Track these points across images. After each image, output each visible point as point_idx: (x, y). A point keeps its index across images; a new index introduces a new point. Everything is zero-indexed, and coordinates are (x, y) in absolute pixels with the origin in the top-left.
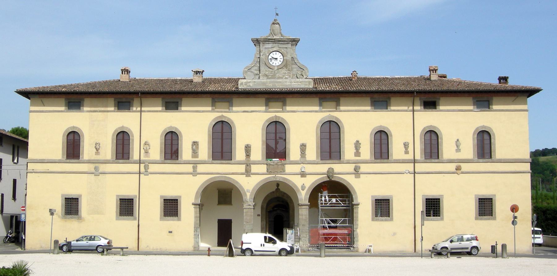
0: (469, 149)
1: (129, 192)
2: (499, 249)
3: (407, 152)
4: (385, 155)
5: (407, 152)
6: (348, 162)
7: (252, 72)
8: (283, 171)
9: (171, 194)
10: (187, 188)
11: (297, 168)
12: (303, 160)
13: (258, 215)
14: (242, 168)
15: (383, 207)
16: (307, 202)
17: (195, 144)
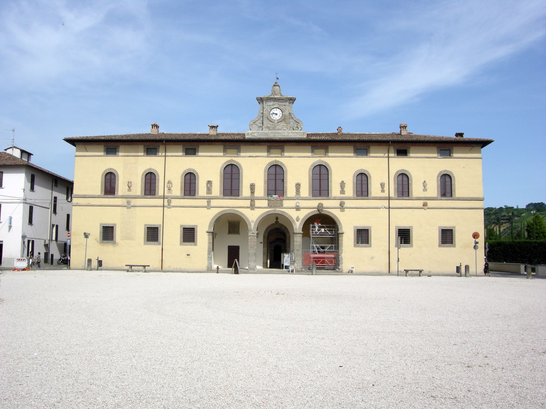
0: (433, 190)
1: (154, 222)
2: (463, 270)
3: (383, 191)
4: (448, 194)
5: (383, 191)
6: (335, 199)
7: (256, 125)
8: (281, 206)
9: (189, 223)
10: (203, 219)
11: (292, 203)
12: (298, 197)
13: (261, 243)
14: (248, 203)
15: (363, 236)
16: (301, 231)
17: (209, 182)
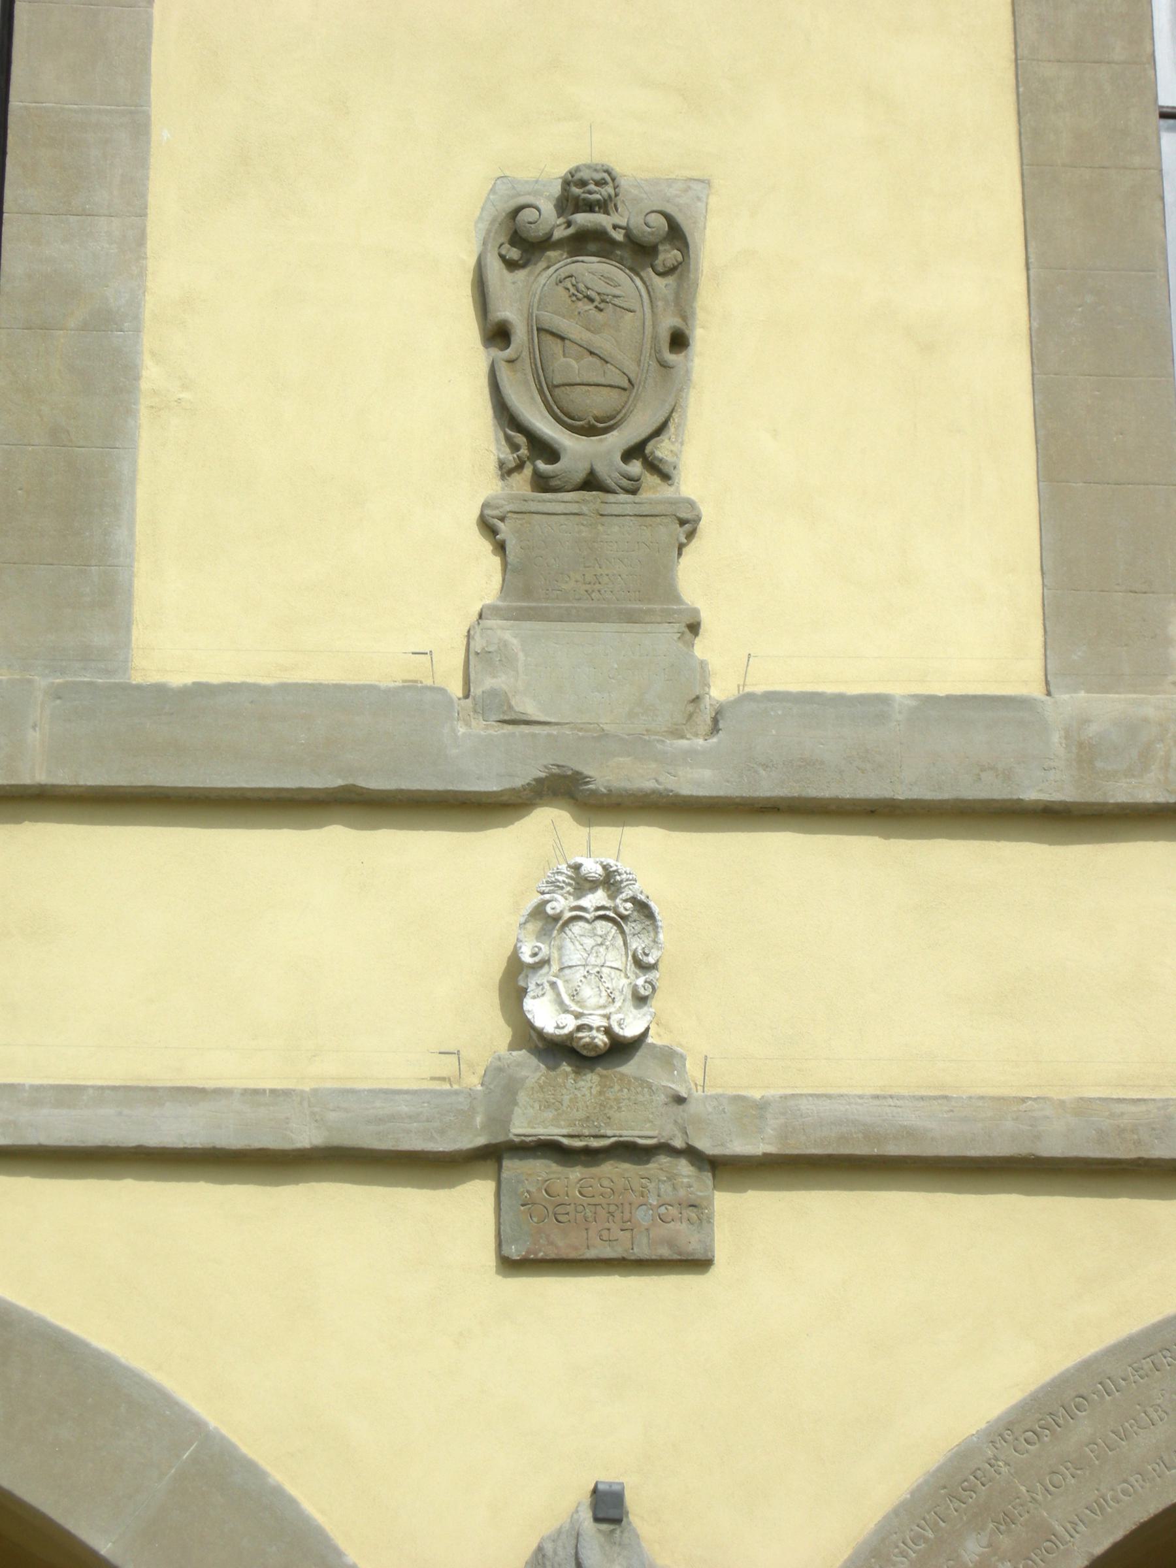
11: (369, 962)
